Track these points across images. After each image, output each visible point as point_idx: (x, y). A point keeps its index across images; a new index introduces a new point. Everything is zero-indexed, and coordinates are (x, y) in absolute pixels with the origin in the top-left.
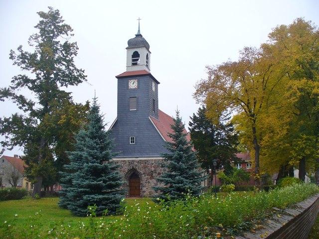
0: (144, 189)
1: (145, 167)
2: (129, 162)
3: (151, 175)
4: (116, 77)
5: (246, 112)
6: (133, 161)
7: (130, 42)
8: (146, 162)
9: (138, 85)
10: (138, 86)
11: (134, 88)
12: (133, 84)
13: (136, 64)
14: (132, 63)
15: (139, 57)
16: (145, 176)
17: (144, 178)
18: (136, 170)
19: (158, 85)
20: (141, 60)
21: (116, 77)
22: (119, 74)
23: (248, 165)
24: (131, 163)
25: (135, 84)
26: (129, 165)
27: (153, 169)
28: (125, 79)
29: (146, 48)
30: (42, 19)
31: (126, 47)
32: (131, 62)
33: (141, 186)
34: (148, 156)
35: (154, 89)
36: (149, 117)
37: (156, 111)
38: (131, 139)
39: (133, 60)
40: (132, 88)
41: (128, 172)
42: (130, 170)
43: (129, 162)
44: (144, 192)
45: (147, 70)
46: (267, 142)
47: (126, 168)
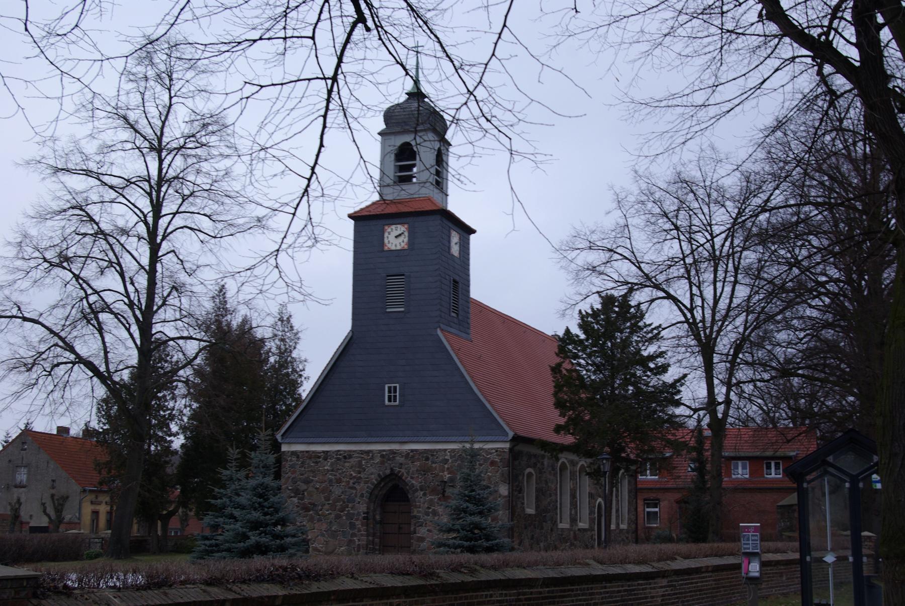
0: (422, 531)
1: (424, 471)
2: (382, 456)
3: (441, 490)
4: (350, 216)
5: (761, 408)
6: (393, 452)
7: (390, 116)
8: (427, 455)
9: (411, 246)
10: (411, 242)
11: (399, 248)
12: (395, 238)
13: (408, 179)
14: (400, 177)
15: (415, 159)
16: (425, 494)
17: (421, 501)
18: (400, 478)
19: (472, 237)
20: (421, 171)
21: (350, 216)
22: (357, 209)
23: (769, 467)
24: (388, 456)
25: (401, 239)
26: (382, 463)
27: (447, 476)
28: (345, 52)
29: (435, 131)
30: (281, 514)
31: (379, 130)
32: (391, 172)
33: (413, 521)
34: (434, 439)
35: (455, 250)
36: (439, 332)
37: (461, 313)
38: (390, 392)
39: (402, 169)
40: (393, 248)
41: (379, 483)
42: (383, 479)
43: (382, 456)
44: (422, 539)
45: (435, 195)
46: (846, 8)
47: (373, 473)
